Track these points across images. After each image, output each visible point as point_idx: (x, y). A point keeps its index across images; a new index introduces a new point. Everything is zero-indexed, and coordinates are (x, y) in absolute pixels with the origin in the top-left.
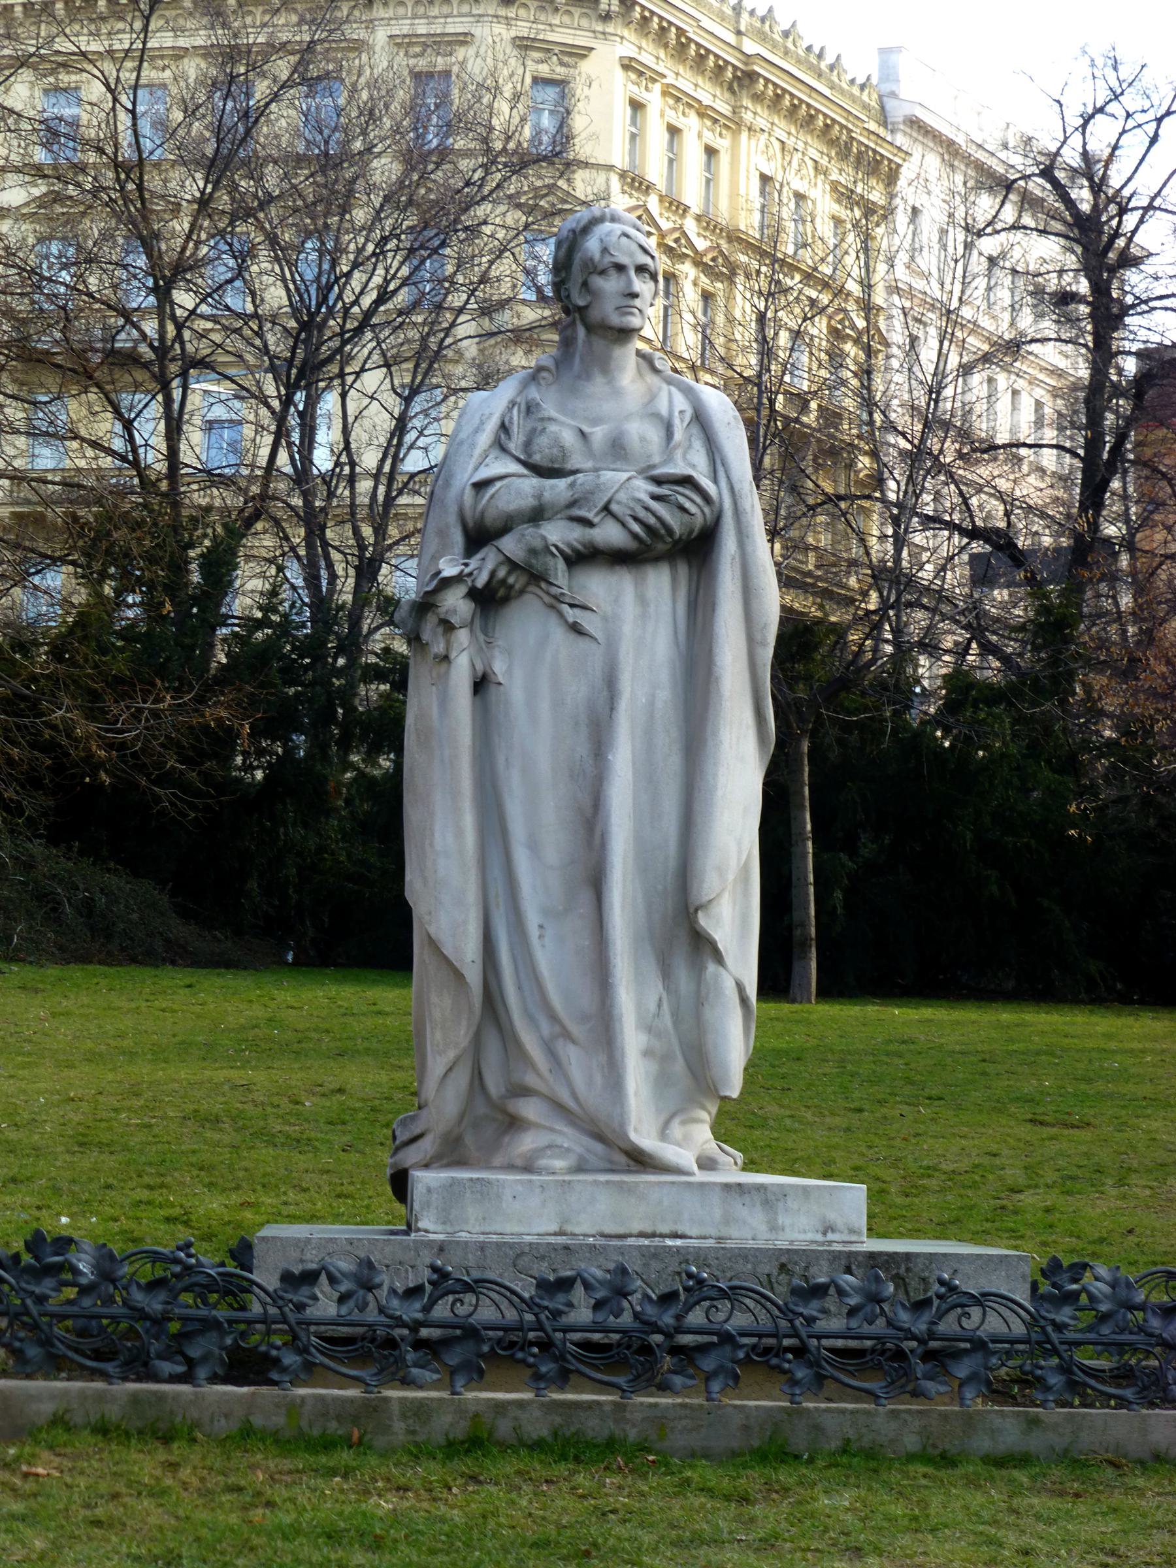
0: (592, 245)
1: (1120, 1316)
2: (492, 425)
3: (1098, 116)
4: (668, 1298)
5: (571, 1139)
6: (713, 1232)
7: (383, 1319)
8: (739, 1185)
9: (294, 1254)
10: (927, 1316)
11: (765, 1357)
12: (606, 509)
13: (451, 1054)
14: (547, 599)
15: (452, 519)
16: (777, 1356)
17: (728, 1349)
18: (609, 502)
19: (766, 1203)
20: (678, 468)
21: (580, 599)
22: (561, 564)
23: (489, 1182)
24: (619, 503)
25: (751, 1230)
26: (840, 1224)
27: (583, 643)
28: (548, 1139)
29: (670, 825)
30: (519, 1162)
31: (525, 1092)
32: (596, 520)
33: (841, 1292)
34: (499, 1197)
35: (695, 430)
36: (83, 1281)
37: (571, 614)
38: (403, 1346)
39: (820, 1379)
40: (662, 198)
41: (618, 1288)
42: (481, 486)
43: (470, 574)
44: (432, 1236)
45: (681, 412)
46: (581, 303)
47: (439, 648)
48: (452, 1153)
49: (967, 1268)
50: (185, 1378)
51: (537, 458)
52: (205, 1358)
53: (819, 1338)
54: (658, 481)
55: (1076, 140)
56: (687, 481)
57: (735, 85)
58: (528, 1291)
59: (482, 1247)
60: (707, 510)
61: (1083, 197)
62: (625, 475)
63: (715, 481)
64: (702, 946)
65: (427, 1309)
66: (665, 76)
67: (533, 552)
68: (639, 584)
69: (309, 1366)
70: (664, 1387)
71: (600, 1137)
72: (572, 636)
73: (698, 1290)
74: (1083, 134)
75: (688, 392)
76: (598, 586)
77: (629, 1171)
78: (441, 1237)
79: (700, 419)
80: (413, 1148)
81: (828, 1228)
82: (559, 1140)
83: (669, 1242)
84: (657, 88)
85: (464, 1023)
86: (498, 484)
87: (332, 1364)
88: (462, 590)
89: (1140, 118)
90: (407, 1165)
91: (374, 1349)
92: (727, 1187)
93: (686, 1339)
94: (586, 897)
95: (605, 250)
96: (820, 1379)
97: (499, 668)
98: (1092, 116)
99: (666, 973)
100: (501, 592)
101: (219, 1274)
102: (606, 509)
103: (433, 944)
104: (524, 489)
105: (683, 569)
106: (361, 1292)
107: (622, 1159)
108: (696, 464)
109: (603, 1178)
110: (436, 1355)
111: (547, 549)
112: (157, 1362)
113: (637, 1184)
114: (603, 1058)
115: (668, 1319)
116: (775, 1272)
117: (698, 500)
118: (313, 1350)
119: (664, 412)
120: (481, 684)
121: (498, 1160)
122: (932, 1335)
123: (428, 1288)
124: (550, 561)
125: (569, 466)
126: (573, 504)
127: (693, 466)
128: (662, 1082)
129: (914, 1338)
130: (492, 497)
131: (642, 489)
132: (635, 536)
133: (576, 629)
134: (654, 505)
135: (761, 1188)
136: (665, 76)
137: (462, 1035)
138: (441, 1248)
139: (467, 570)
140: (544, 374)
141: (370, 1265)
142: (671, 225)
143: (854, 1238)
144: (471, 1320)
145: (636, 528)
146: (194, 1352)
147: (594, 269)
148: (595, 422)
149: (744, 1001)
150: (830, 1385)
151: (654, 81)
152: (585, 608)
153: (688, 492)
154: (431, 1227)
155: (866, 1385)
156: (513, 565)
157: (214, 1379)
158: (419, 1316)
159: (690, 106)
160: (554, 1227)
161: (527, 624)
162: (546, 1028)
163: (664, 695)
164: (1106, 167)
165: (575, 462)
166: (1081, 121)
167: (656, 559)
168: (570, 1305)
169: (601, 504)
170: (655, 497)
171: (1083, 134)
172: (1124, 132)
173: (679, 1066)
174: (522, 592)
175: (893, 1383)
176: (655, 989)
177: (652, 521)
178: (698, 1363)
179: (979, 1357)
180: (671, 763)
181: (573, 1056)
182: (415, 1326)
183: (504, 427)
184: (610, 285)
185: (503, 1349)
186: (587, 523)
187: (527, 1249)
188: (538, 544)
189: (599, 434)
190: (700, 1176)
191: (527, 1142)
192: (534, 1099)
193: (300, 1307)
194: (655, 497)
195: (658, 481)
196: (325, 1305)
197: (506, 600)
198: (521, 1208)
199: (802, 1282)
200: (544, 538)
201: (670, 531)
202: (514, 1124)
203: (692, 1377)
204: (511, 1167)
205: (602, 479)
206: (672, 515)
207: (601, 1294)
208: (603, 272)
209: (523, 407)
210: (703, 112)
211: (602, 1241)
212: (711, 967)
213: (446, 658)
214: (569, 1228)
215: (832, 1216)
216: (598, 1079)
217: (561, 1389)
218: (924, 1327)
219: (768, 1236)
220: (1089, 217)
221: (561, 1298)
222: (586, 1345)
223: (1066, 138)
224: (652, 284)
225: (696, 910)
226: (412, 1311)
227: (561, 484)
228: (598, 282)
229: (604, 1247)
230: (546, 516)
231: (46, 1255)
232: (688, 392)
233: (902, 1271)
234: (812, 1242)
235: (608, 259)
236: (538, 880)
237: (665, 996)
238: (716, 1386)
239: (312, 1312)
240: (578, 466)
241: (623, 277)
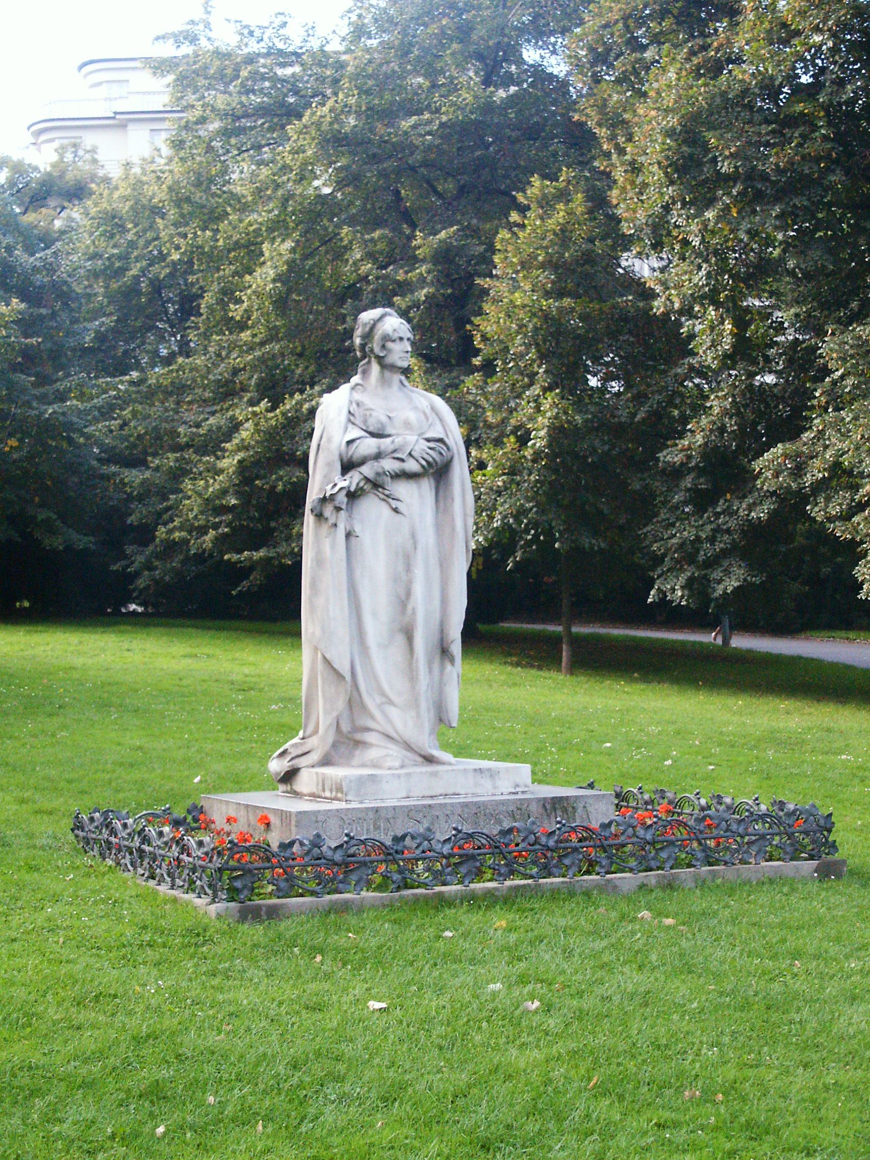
12: (410, 454)
14: (382, 496)
21: (397, 496)
29: (437, 602)
37: (394, 504)
42: (349, 443)
47: (332, 521)
49: (590, 801)
51: (371, 429)
54: (428, 440)
67: (378, 474)
68: (419, 487)
76: (402, 489)
79: (433, 409)
82: (391, 752)
94: (400, 639)
97: (358, 529)
102: (410, 454)
104: (369, 446)
107: (420, 759)
111: (384, 473)
114: (413, 713)
120: (348, 535)
126: (395, 451)
131: (424, 445)
132: (423, 466)
133: (396, 510)
145: (424, 463)
156: (367, 480)
161: (372, 508)
162: (379, 699)
165: (389, 430)
179: (671, 849)
180: (436, 574)
186: (402, 460)
188: (380, 470)
195: (428, 440)
208: (394, 341)
213: (336, 525)
215: (518, 781)
227: (388, 441)
228: (390, 345)
231: (864, 886)
235: (396, 335)
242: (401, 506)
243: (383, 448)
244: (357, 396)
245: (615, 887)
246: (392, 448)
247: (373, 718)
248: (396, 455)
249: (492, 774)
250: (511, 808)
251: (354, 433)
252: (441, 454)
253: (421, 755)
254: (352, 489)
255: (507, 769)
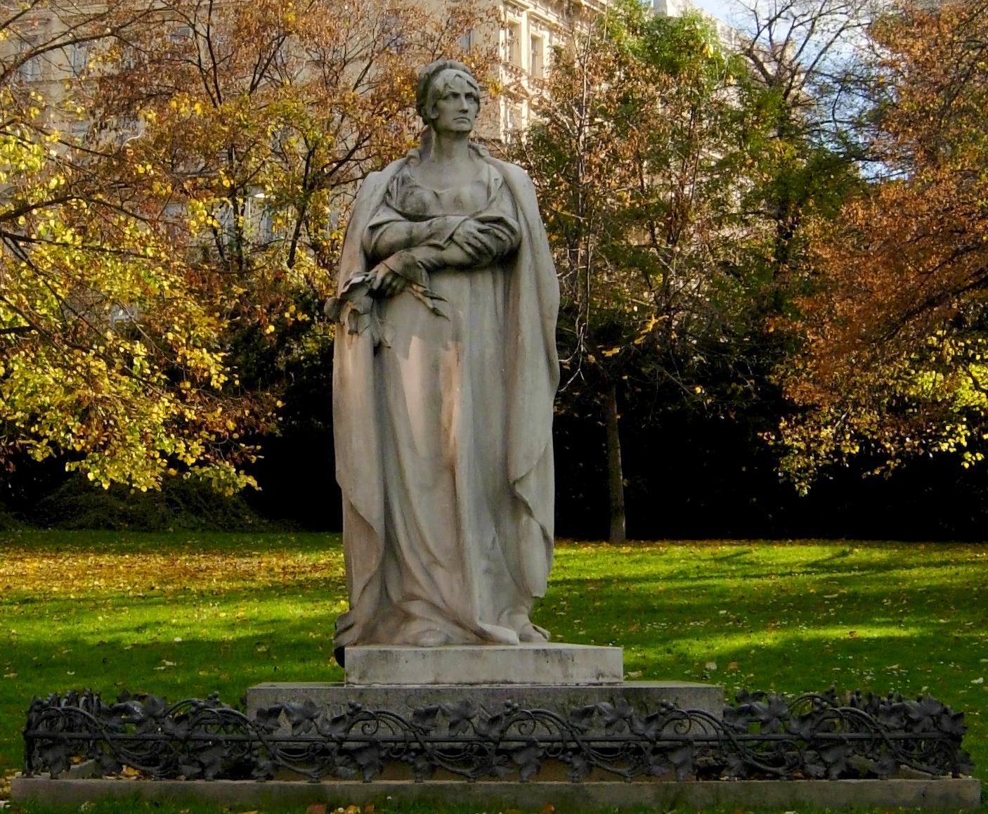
0: (439, 83)
1: (774, 722)
2: (381, 191)
3: (778, 20)
4: (494, 720)
5: (440, 625)
6: (529, 679)
7: (320, 737)
8: (544, 650)
9: (271, 699)
10: (654, 726)
11: (553, 756)
12: (451, 238)
13: (367, 576)
15: (358, 247)
16: (563, 753)
17: (532, 750)
18: (453, 234)
19: (561, 660)
20: (493, 213)
21: (437, 294)
22: (424, 273)
23: (390, 652)
24: (459, 235)
25: (552, 676)
26: (607, 673)
27: (440, 320)
28: (427, 627)
29: (497, 430)
30: (410, 640)
31: (413, 597)
32: (445, 246)
33: (601, 713)
34: (397, 661)
35: (504, 190)
36: (137, 718)
38: (333, 753)
39: (590, 767)
40: (529, 78)
41: (462, 717)
42: (374, 228)
43: (370, 281)
44: (356, 687)
45: (496, 180)
46: (433, 117)
48: (369, 636)
50: (201, 776)
51: (408, 210)
52: (212, 764)
53: (589, 741)
54: (482, 221)
55: (765, 33)
56: (500, 221)
57: (571, 11)
58: (408, 716)
59: (387, 692)
60: (513, 238)
61: (771, 69)
62: (463, 218)
63: (517, 220)
64: (518, 505)
65: (347, 731)
66: (527, 8)
69: (276, 767)
70: (493, 776)
71: (459, 624)
72: (433, 317)
73: (512, 714)
74: (770, 29)
75: (500, 168)
76: (448, 286)
77: (477, 644)
78: (363, 687)
79: (507, 184)
80: (347, 633)
81: (600, 675)
82: (434, 626)
83: (502, 686)
84: (524, 14)
85: (374, 557)
86: (385, 226)
87: (290, 766)
88: (364, 291)
89: (802, 19)
90: (343, 644)
91: (318, 756)
92: (537, 651)
93: (351, 745)
94: (446, 477)
95: (446, 85)
96: (590, 767)
97: (388, 338)
98: (775, 19)
99: (497, 524)
100: (389, 291)
101: (220, 712)
103: (353, 508)
104: (399, 230)
105: (500, 275)
106: (307, 721)
107: (473, 637)
108: (503, 209)
109: (460, 648)
110: (354, 760)
112: (809, 766)
113: (482, 651)
114: (460, 575)
115: (494, 733)
116: (566, 703)
117: (507, 232)
118: (435, 758)
119: (485, 180)
121: (398, 639)
122: (658, 738)
123: (348, 718)
124: (418, 272)
125: (428, 214)
126: (430, 236)
127: (504, 212)
128: (497, 589)
129: (648, 740)
130: (382, 234)
131: (472, 226)
132: (469, 254)
133: (435, 312)
134: (481, 236)
135: (559, 652)
136: (527, 8)
137: (374, 564)
138: (361, 693)
139: (367, 279)
140: (412, 160)
141: (312, 704)
142: (535, 93)
143: (615, 680)
144: (375, 736)
145: (469, 249)
146: (828, 758)
147: (439, 96)
148: (442, 187)
149: (546, 537)
150: (596, 771)
151: (522, 10)
152: (440, 299)
153: (501, 227)
154: (356, 681)
155: (619, 770)
157: (218, 776)
158: (342, 735)
159: (544, 24)
160: (432, 679)
162: (425, 558)
163: (490, 351)
164: (783, 50)
165: (433, 210)
166: (767, 22)
167: (482, 269)
168: (278, 725)
169: (447, 236)
170: (481, 231)
171: (770, 29)
172: (793, 27)
173: (507, 579)
174: (402, 291)
175: (635, 767)
176: (491, 533)
177: (479, 245)
178: (515, 759)
181: (439, 574)
182: (341, 741)
183: (388, 192)
184: (450, 106)
185: (551, 753)
187: (413, 693)
188: (409, 261)
189: (446, 194)
190: (521, 646)
191: (414, 628)
192: (419, 602)
193: (270, 731)
194: (481, 231)
195: (482, 221)
196: (284, 728)
197: (392, 296)
198: (417, 666)
199: (578, 706)
200: (413, 258)
201: (490, 251)
202: (408, 617)
203: (511, 768)
204: (406, 643)
205: (448, 221)
206: (491, 240)
207: (453, 718)
208: (446, 98)
209: (400, 180)
210: (553, 29)
211: (460, 687)
212: (525, 518)
214: (440, 679)
215: (602, 668)
216: (457, 588)
217: (431, 778)
218: (653, 733)
219: (563, 681)
220: (775, 78)
221: (272, 720)
222: (603, 751)
223: (759, 33)
224: (476, 105)
225: (514, 483)
226: (338, 732)
227: (424, 224)
228: (442, 104)
229: (461, 690)
230: (416, 243)
232: (500, 168)
233: (644, 699)
234: (590, 684)
235: (448, 91)
236: (415, 467)
237: (497, 539)
238: (525, 774)
239: (277, 734)
240: (434, 214)
241: (458, 100)
242: (440, 306)
243: (415, 232)
244: (406, 172)
245: (588, 797)
246: (427, 232)
247: (417, 582)
248: (432, 241)
249: (562, 658)
250: (560, 701)
251: (384, 215)
252: (498, 237)
253: (475, 633)
254: (375, 287)
255: (594, 650)
